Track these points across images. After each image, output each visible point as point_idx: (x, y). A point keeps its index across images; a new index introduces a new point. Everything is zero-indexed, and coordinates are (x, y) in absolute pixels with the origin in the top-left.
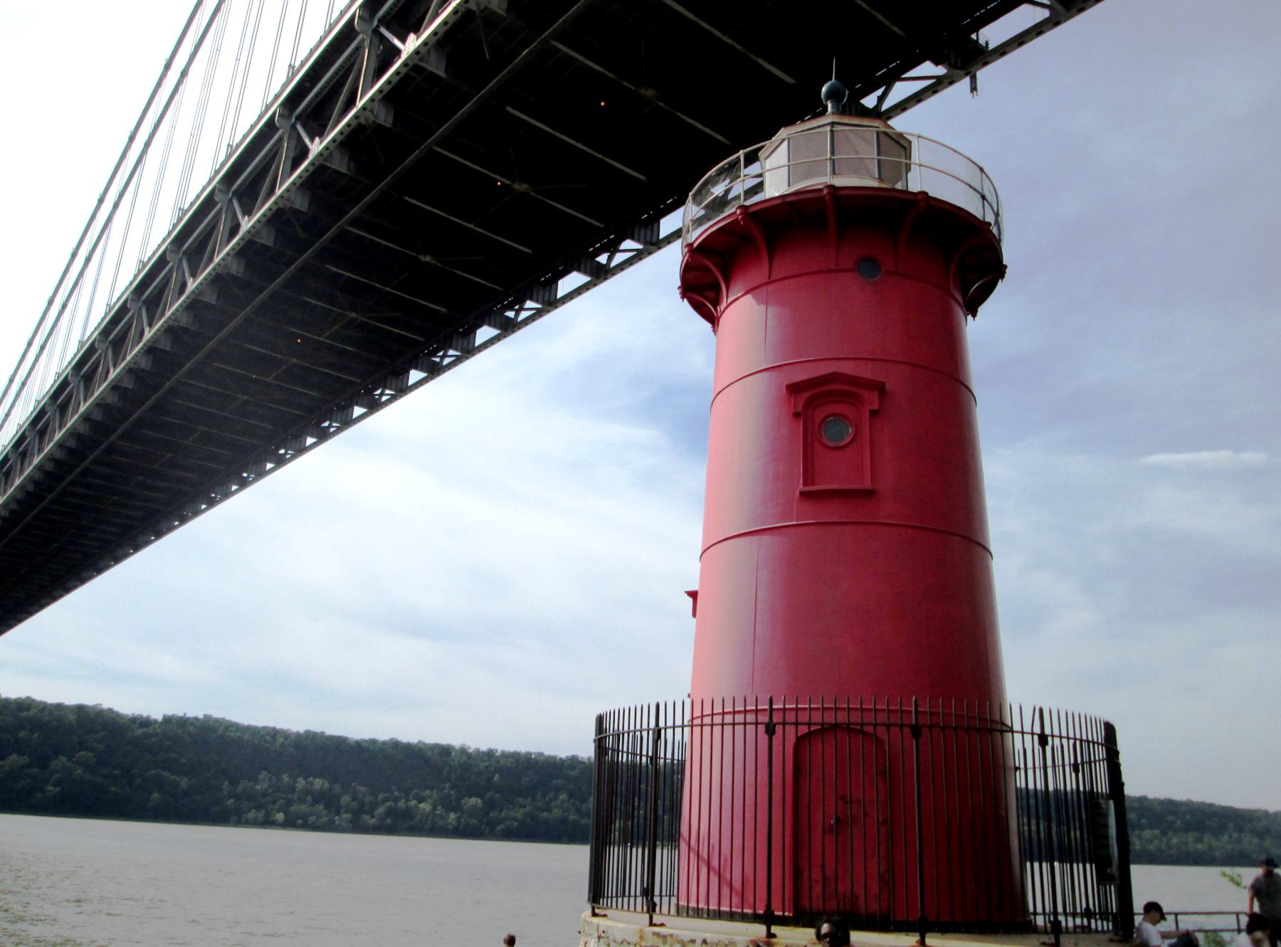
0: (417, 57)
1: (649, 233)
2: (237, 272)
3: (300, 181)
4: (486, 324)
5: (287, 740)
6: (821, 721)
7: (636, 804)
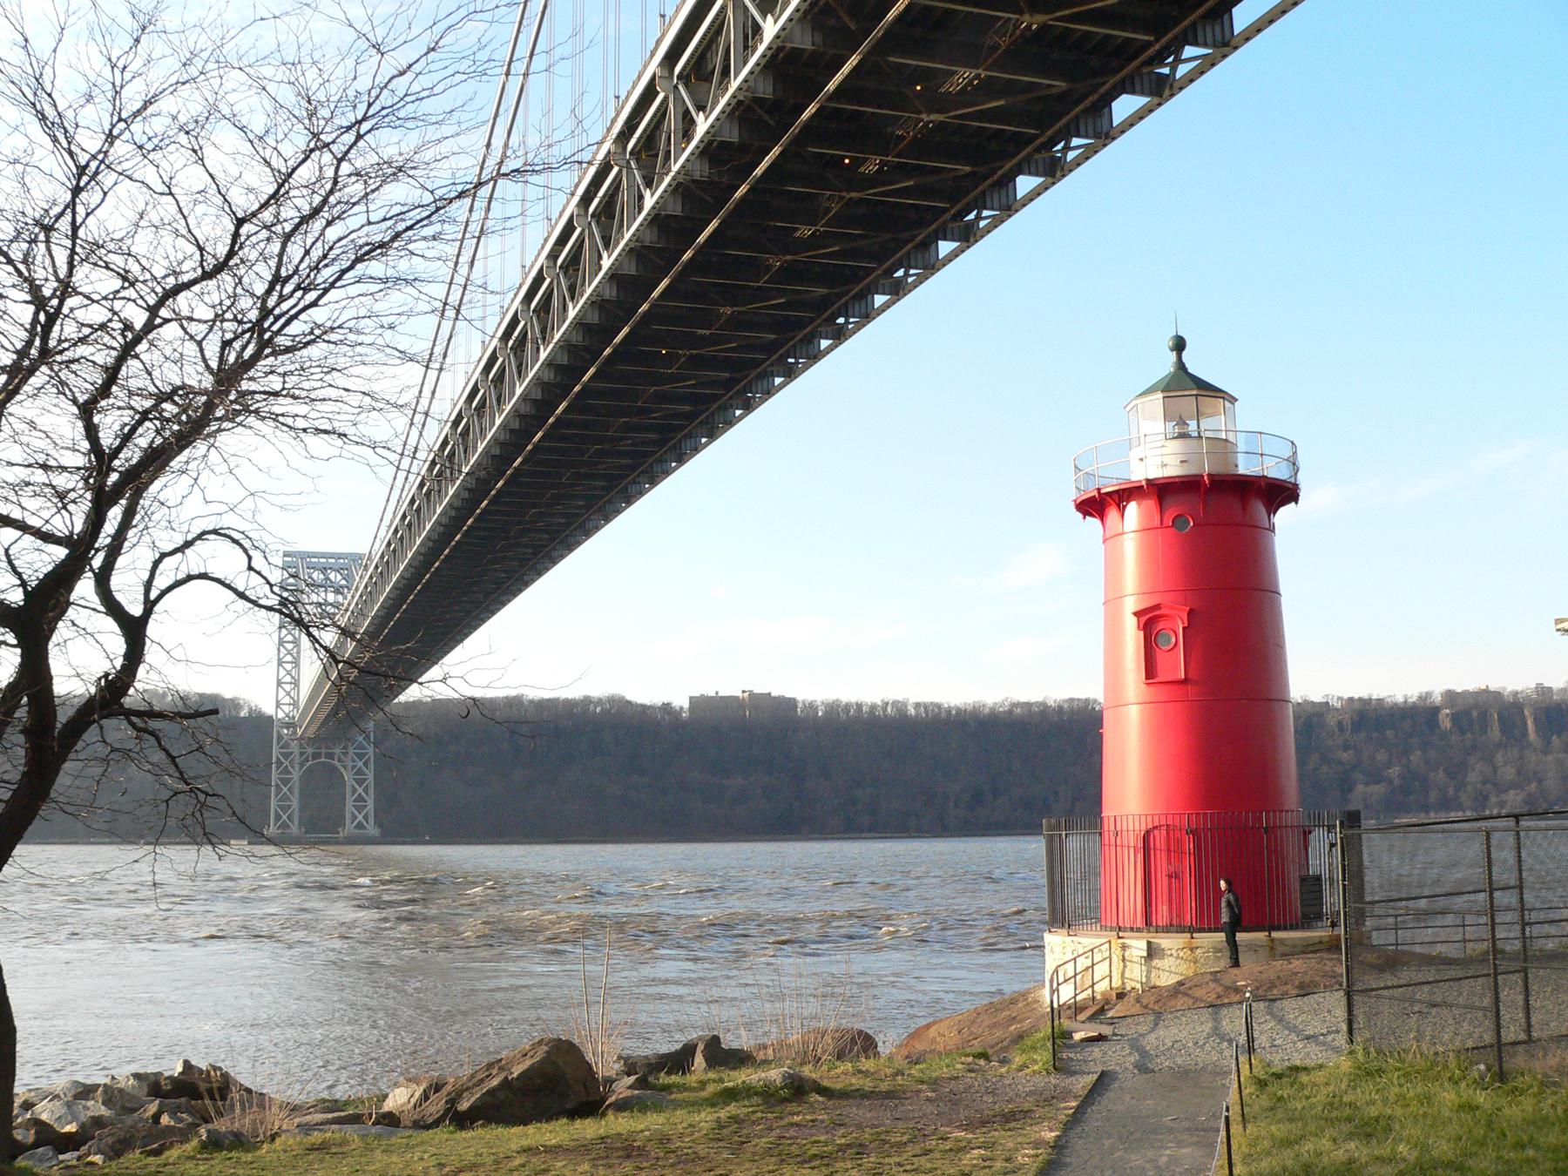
1: (1218, 29)
2: (764, 93)
3: (698, 151)
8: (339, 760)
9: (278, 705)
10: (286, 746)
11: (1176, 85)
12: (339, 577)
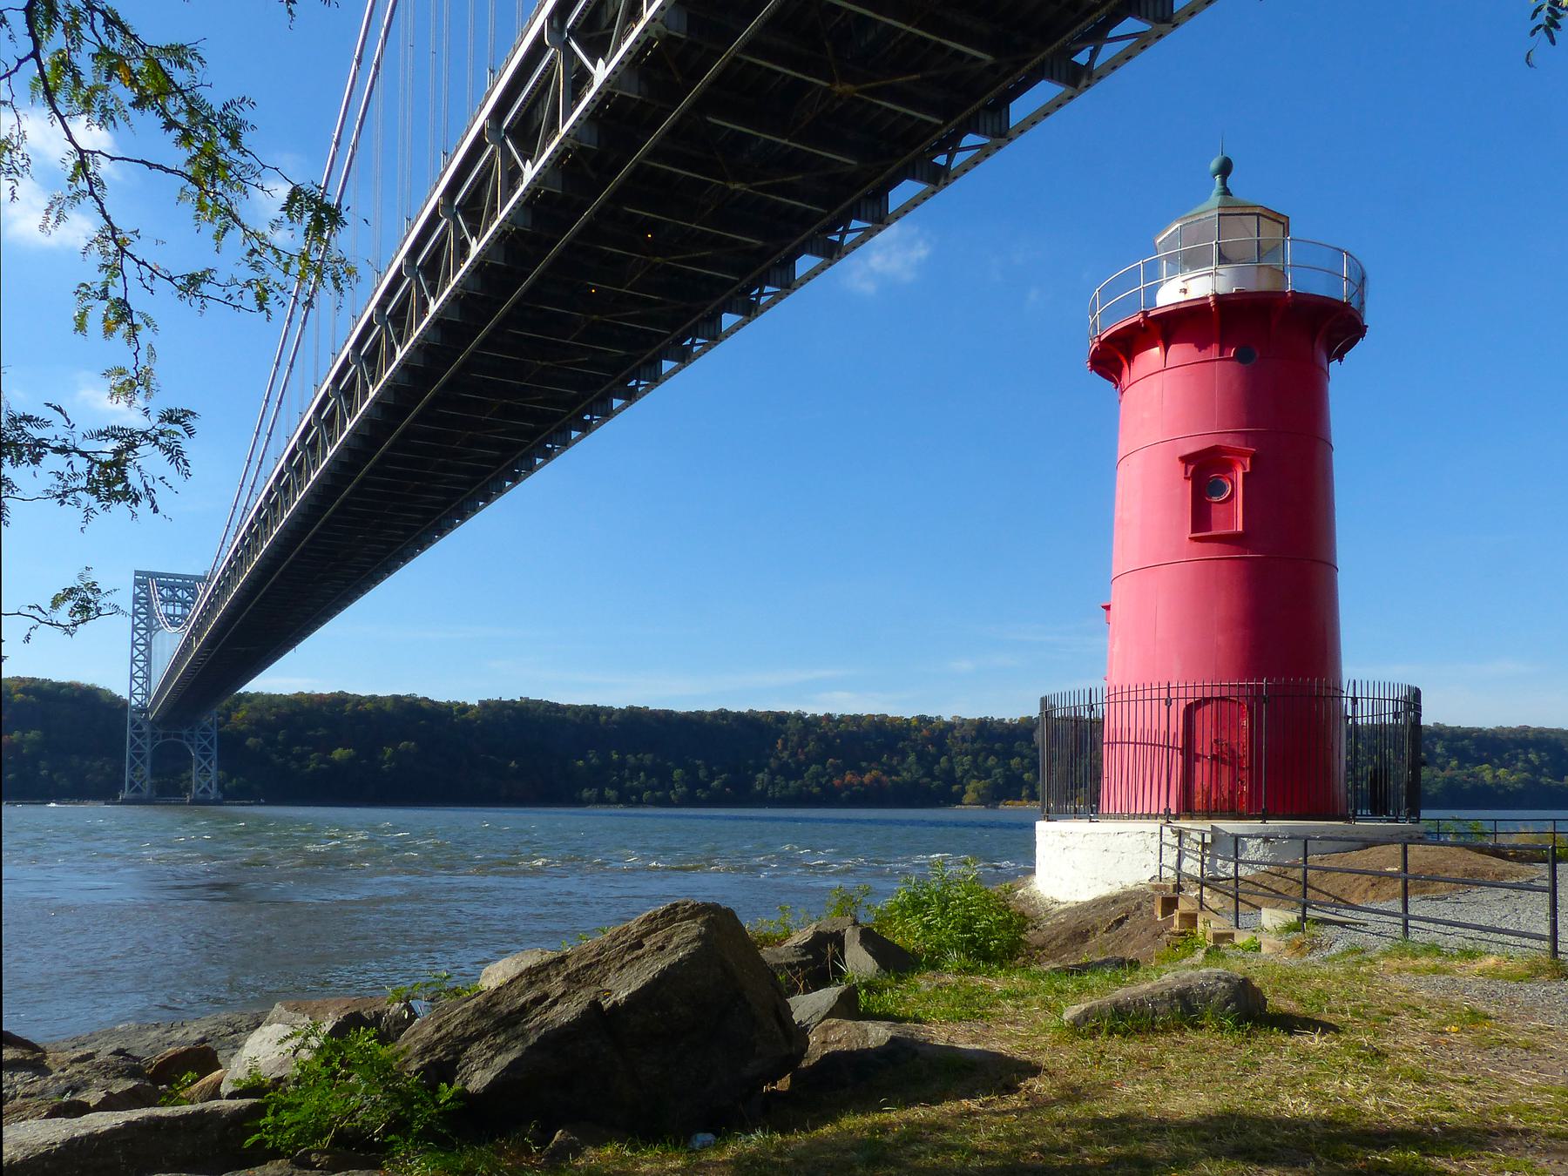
0: (535, 183)
4: (806, 252)
5: (611, 718)
7: (1078, 762)
8: (187, 740)
9: (132, 694)
10: (139, 727)
11: (843, 251)
12: (186, 594)
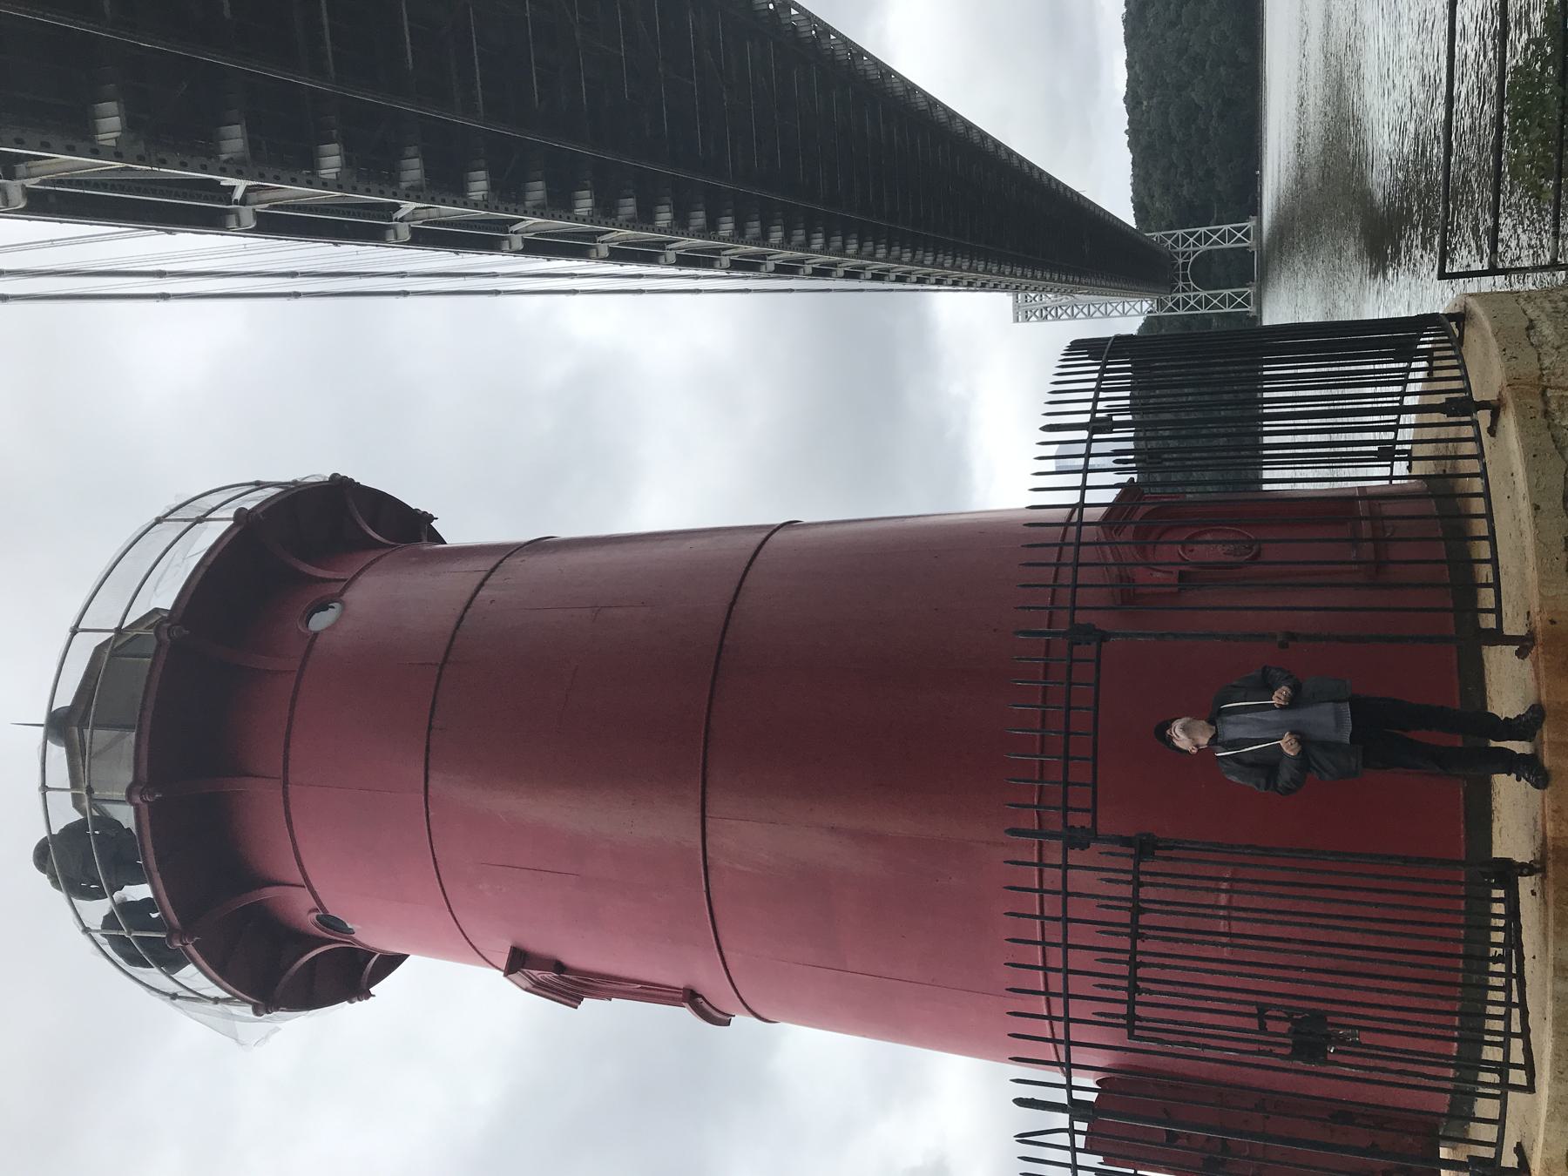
0: (244, 169)
6: (1070, 568)
8: (1189, 257)
9: (1141, 313)
